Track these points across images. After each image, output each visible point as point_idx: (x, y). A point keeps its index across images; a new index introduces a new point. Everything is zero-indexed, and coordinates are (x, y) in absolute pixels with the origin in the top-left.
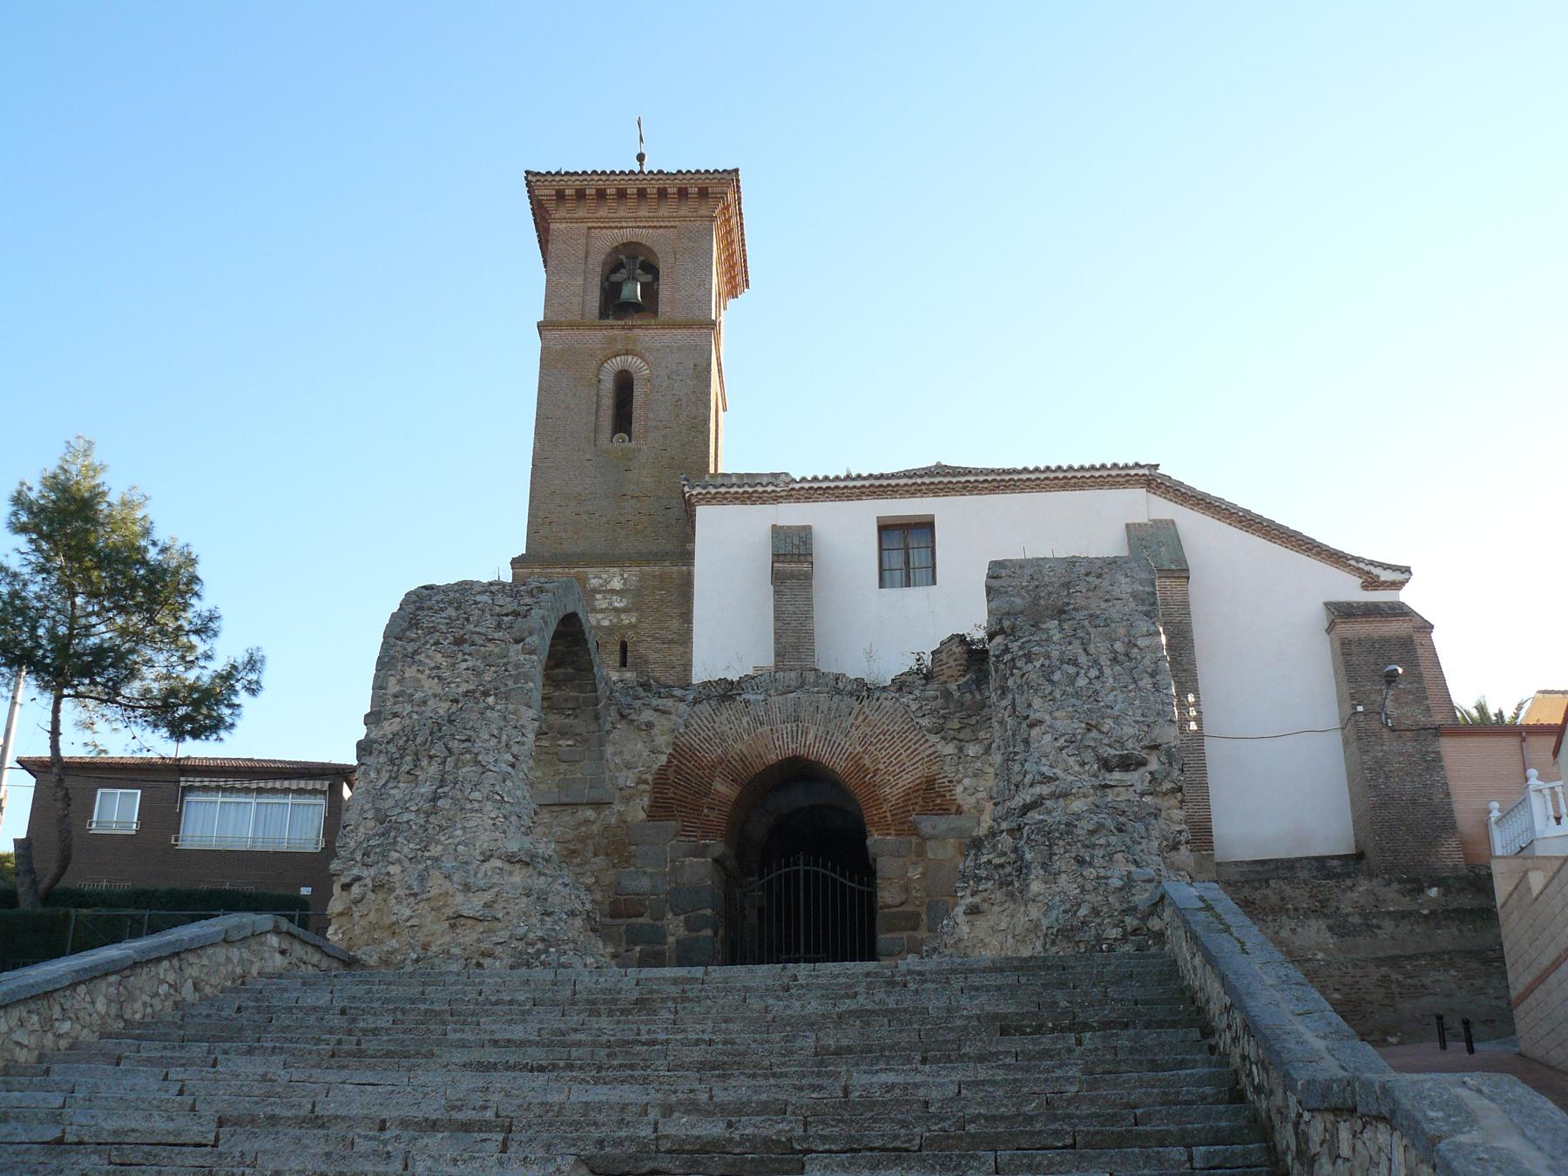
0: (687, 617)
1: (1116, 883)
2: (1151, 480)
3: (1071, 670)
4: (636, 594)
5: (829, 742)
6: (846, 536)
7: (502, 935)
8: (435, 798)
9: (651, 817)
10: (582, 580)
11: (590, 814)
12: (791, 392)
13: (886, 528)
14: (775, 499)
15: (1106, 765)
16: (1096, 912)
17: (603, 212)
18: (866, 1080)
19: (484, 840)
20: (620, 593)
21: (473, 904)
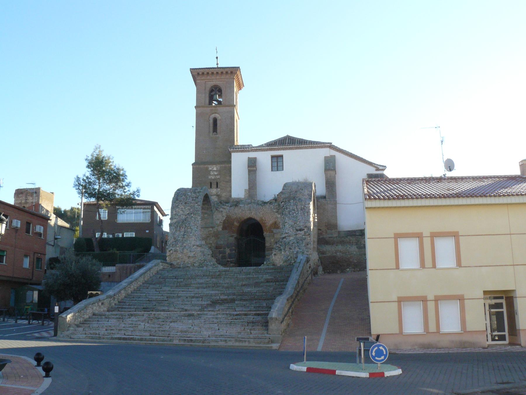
0: (230, 176)
1: (295, 252)
2: (330, 146)
3: (293, 212)
4: (219, 172)
5: (257, 214)
6: (264, 159)
7: (197, 260)
8: (184, 235)
9: (223, 229)
10: (207, 168)
11: (211, 229)
12: (253, 124)
13: (273, 157)
14: (249, 151)
15: (297, 230)
16: (291, 258)
17: (208, 78)
18: (247, 290)
19: (193, 243)
20: (216, 171)
21: (192, 254)
